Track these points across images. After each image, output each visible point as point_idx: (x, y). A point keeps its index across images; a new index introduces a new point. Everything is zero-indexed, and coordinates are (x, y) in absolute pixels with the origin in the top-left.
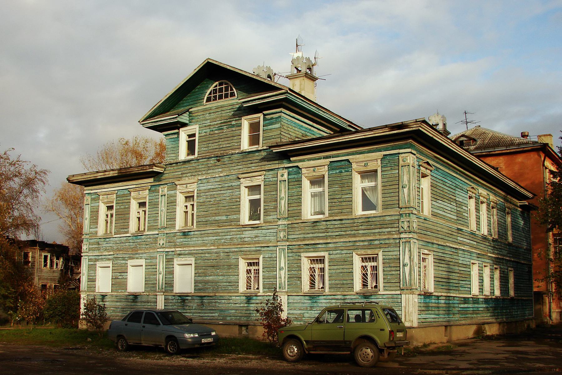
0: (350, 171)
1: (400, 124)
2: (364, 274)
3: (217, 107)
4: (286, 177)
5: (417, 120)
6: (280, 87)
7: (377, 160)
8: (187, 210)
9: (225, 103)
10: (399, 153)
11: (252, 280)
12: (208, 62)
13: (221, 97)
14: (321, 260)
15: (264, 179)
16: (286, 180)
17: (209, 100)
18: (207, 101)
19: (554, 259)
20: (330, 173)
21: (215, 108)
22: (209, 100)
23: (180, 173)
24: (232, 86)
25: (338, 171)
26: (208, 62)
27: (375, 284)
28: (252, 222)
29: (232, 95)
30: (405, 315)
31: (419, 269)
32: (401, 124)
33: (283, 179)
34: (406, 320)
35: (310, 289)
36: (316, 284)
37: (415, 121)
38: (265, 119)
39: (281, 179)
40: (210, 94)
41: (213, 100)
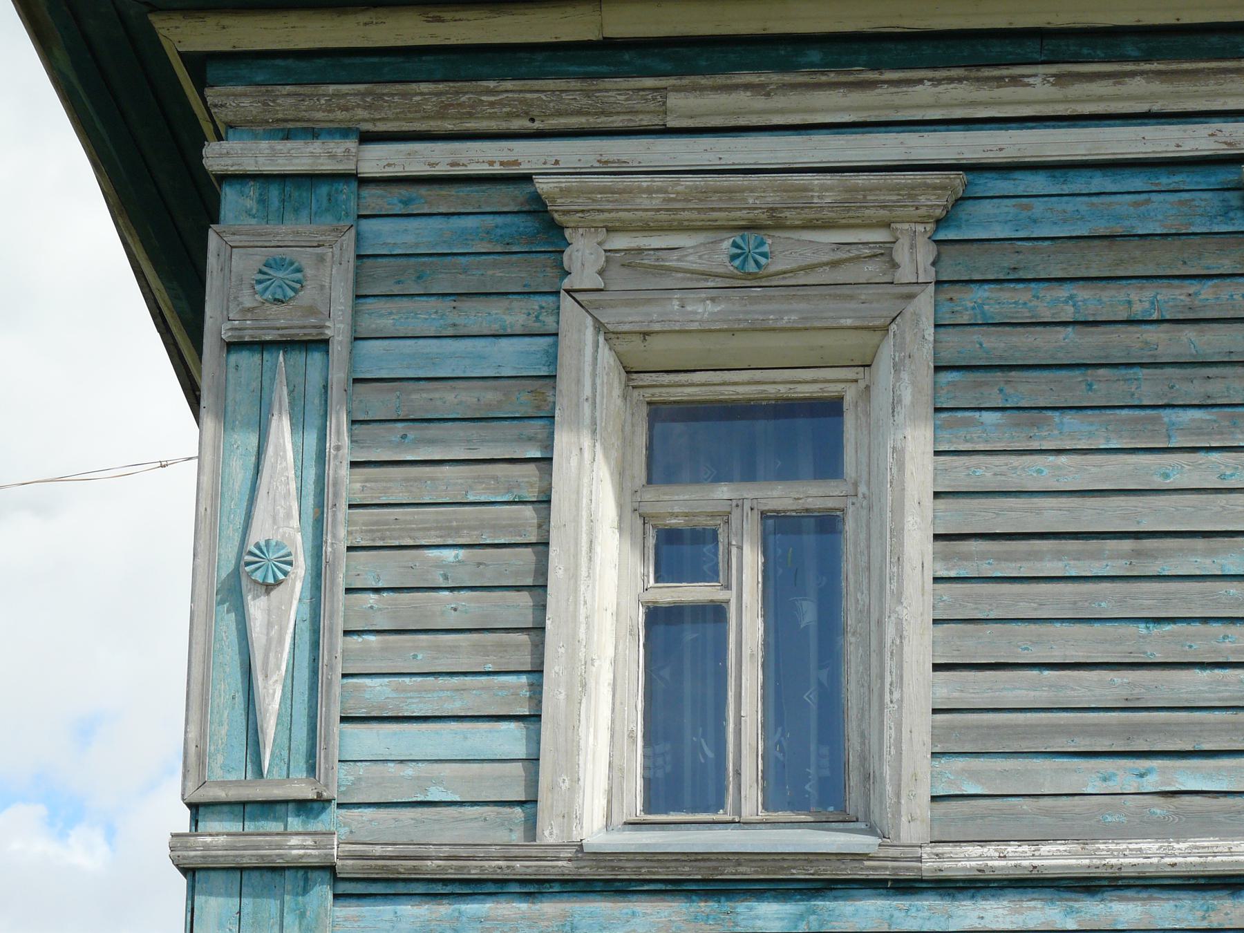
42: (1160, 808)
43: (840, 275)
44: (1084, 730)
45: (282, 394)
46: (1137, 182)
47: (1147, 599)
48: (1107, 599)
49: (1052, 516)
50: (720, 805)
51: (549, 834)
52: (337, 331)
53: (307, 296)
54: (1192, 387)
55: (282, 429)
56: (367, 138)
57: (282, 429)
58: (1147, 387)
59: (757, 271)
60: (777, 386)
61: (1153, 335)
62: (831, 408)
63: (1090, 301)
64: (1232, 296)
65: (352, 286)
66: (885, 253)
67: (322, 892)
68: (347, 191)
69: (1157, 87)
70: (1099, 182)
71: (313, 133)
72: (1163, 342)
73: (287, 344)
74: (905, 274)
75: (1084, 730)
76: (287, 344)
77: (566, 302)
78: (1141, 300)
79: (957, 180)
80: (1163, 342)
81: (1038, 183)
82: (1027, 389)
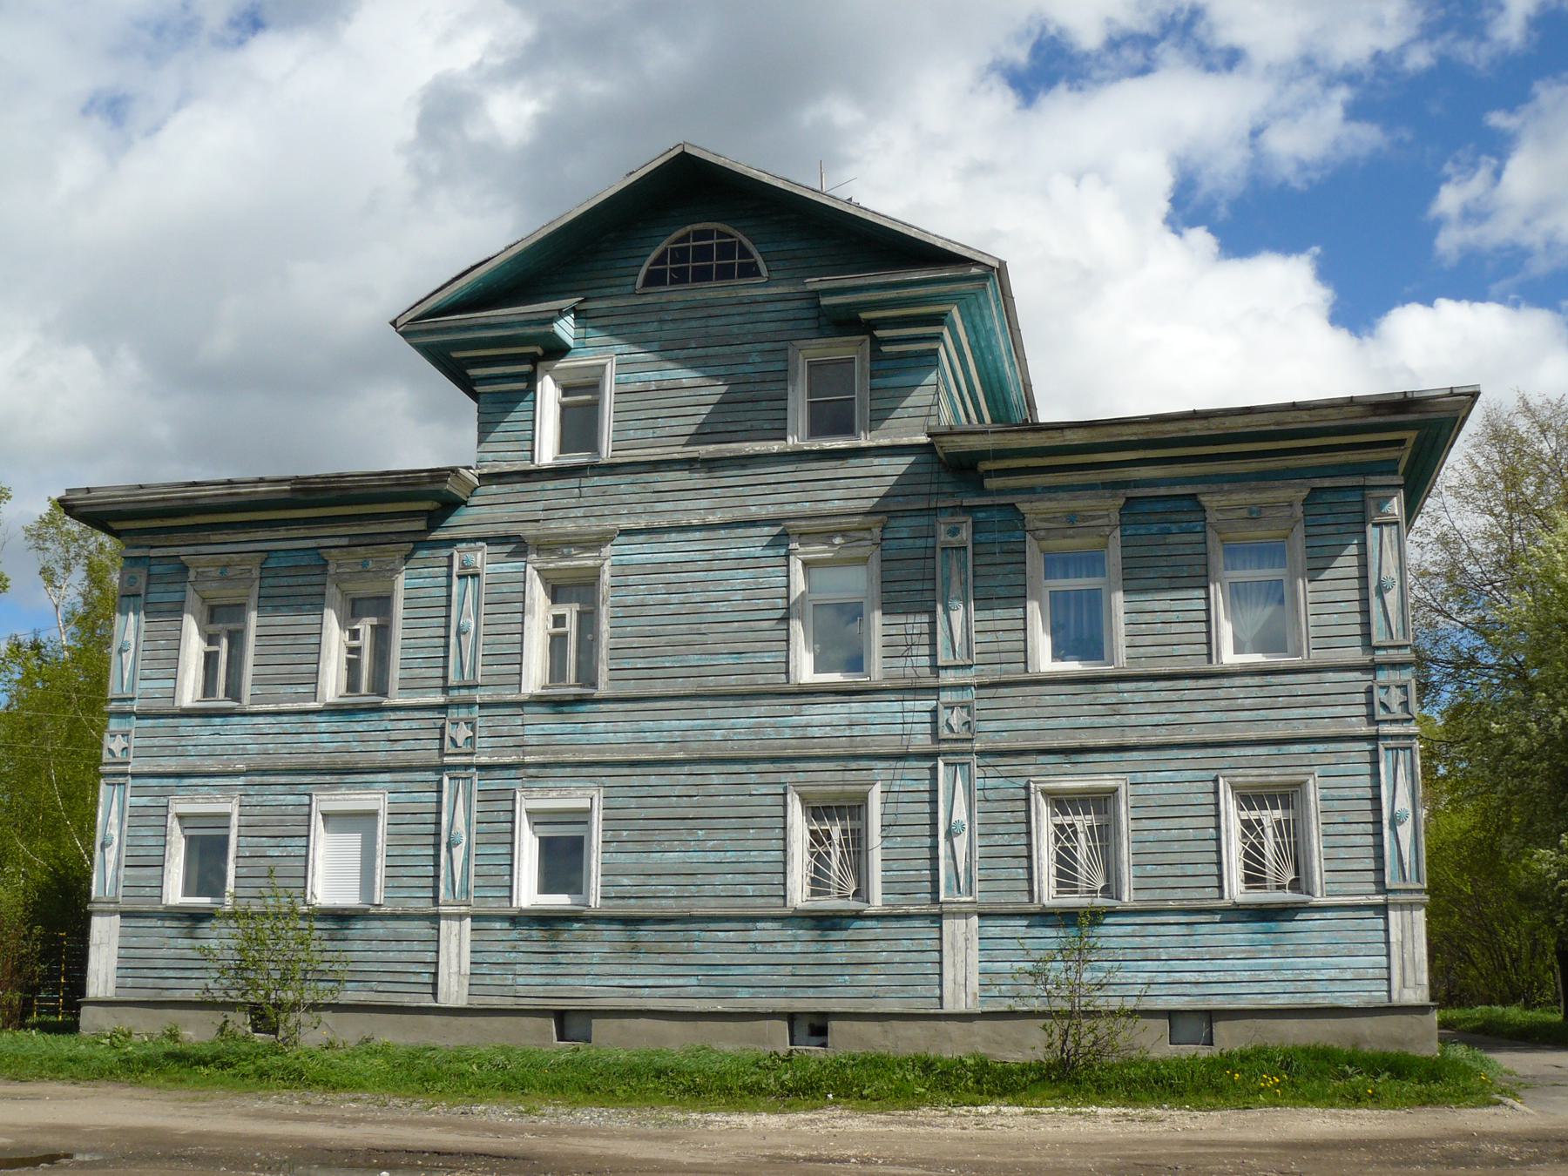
0: (1198, 529)
1: (1397, 397)
2: (1252, 846)
3: (688, 305)
4: (965, 534)
5: (1455, 391)
6: (967, 254)
7: (1291, 505)
8: (355, 643)
9: (722, 294)
10: (1364, 487)
11: (835, 863)
12: (683, 152)
13: (703, 275)
14: (1101, 801)
15: (882, 539)
16: (965, 548)
17: (654, 279)
18: (648, 282)
19: (1285, 807)
20: (1128, 533)
21: (681, 305)
22: (654, 279)
23: (540, 505)
24: (746, 241)
25: (1155, 529)
26: (683, 152)
27: (1294, 877)
28: (1073, 667)
29: (750, 271)
30: (1403, 969)
31: (148, 836)
32: (1402, 396)
33: (954, 541)
34: (1407, 984)
35: (1058, 892)
36: (1082, 872)
37: (1448, 392)
38: (876, 355)
39: (949, 542)
40: (661, 260)
41: (673, 282)
42: (294, 696)
43: (243, 576)
44: (281, 679)
45: (132, 606)
46: (302, 553)
47: (296, 649)
48: (288, 649)
49: (279, 630)
50: (214, 696)
51: (176, 705)
52: (143, 592)
53: (138, 584)
54: (309, 600)
55: (131, 614)
56: (152, 547)
57: (131, 614)
58: (300, 600)
59: (781, 528)
60: (232, 601)
61: (302, 588)
62: (244, 605)
63: (290, 581)
64: (475, 576)
65: (107, 1123)
66: (250, 570)
67: (134, 718)
68: (147, 560)
69: (307, 531)
70: (295, 553)
71: (141, 547)
72: (304, 590)
73: (133, 596)
74: (254, 576)
75: (281, 679)
76: (133, 596)
77: (188, 584)
78: (300, 580)
79: (265, 555)
80: (304, 590)
81: (282, 554)
82: (277, 602)
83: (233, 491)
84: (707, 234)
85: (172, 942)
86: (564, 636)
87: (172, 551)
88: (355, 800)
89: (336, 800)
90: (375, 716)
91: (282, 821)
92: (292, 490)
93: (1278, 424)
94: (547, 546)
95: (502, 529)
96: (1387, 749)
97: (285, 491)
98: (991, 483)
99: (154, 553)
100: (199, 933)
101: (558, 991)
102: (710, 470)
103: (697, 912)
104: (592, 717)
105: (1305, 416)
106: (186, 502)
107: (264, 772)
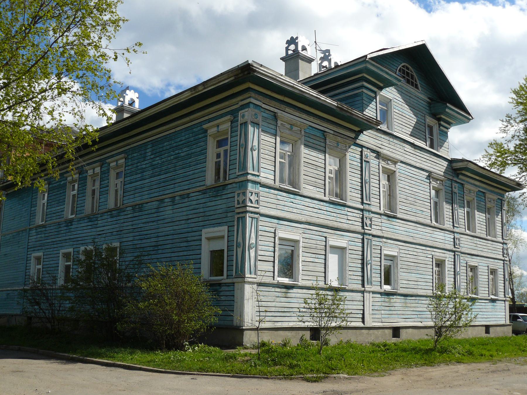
69: (320, 122)
83: (319, 97)
84: (408, 68)
85: (278, 299)
86: (220, 161)
87: (276, 110)
88: (340, 242)
89: (337, 241)
90: (342, 208)
91: (316, 247)
92: (337, 107)
93: (506, 182)
94: (386, 159)
95: (375, 148)
96: (249, 217)
97: (335, 106)
98: (461, 177)
99: (264, 106)
100: (289, 295)
101: (389, 320)
102: (415, 148)
103: (419, 294)
104: (396, 224)
105: (509, 181)
106: (300, 93)
107: (309, 224)
